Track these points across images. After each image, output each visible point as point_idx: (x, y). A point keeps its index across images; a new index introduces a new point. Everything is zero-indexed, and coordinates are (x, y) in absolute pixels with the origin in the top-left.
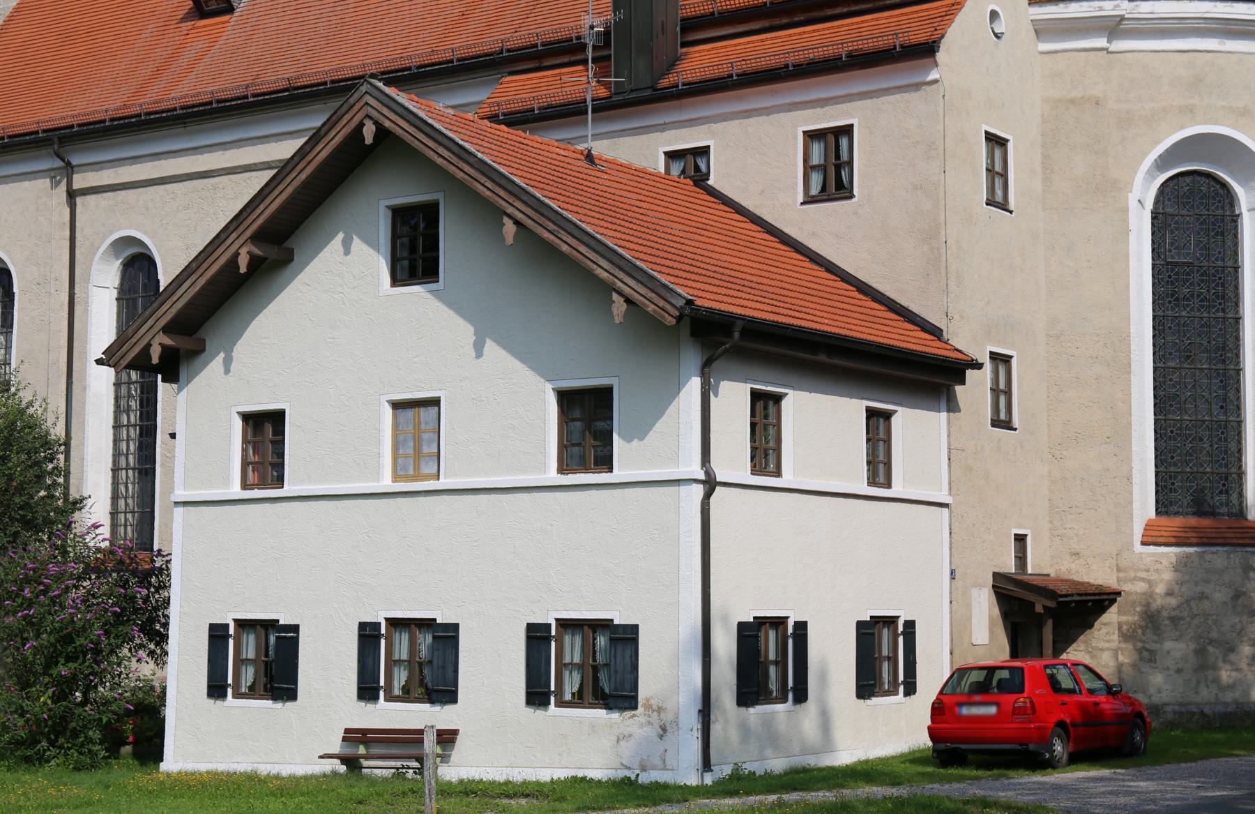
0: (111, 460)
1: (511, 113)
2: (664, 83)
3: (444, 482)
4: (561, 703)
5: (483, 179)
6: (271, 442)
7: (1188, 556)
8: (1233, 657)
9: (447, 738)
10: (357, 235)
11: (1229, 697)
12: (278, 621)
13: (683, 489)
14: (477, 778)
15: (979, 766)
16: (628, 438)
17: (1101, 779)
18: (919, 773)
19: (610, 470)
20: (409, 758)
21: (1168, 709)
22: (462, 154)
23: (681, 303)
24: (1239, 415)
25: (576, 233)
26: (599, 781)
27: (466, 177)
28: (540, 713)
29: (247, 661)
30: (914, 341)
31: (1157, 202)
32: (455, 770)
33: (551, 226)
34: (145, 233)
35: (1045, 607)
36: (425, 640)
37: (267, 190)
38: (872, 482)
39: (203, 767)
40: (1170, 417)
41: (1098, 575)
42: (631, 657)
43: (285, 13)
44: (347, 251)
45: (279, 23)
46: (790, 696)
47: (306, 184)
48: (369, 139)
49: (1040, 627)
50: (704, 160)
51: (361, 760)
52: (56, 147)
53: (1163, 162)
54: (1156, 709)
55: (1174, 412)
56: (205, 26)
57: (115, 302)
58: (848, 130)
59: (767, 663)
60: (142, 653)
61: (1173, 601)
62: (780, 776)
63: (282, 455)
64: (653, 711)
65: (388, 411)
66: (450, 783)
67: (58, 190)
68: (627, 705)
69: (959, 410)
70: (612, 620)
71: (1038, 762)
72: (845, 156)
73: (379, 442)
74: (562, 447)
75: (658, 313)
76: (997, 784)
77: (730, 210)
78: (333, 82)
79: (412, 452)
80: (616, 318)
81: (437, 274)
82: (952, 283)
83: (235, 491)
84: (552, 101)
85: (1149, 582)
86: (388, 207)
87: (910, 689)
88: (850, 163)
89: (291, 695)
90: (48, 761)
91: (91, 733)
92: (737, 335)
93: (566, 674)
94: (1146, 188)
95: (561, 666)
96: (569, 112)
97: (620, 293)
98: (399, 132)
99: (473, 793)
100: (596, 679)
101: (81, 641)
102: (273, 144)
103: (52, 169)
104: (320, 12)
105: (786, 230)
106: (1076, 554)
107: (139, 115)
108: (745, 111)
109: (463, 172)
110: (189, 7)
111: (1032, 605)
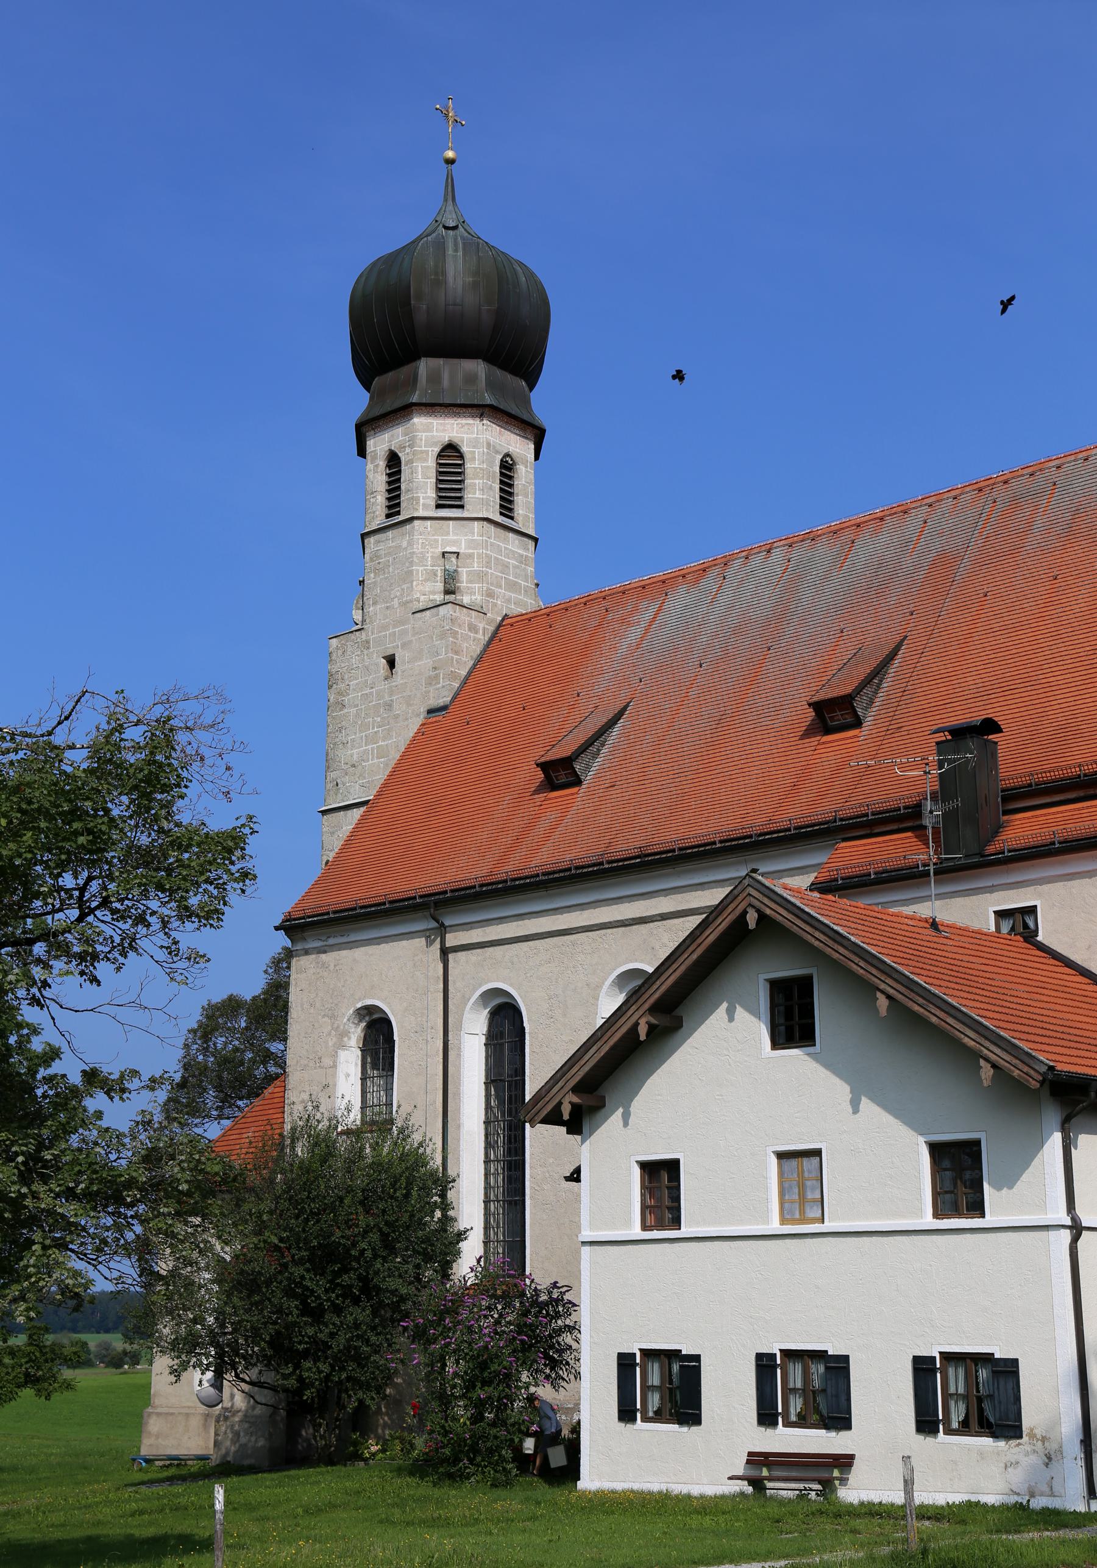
0: (482, 1192)
3: (829, 1226)
4: (949, 1431)
5: (857, 960)
9: (845, 1462)
10: (740, 1004)
12: (681, 1351)
13: (1052, 1234)
14: (876, 1500)
16: (998, 1188)
19: (983, 1215)
20: (813, 1480)
22: (837, 937)
23: (1044, 1069)
25: (945, 1007)
26: (993, 1506)
27: (841, 957)
28: (930, 1440)
29: (653, 1388)
33: (921, 1001)
34: (511, 985)
37: (663, 968)
39: (619, 1486)
42: (1013, 1389)
43: (629, 785)
44: (731, 1019)
45: (624, 794)
48: (752, 925)
50: (1032, 918)
51: (765, 1482)
52: (432, 910)
56: (556, 798)
57: (484, 1048)
60: (541, 1377)
63: (676, 1199)
64: (1038, 1440)
65: (774, 1160)
66: (851, 1504)
67: (432, 948)
68: (1012, 1434)
70: (993, 1354)
73: (767, 1189)
75: (1024, 1078)
77: (1060, 964)
78: (680, 849)
79: (797, 1197)
80: (984, 1081)
83: (636, 1231)
84: (888, 866)
86: (766, 980)
89: (694, 1419)
91: (504, 1452)
93: (952, 1404)
95: (946, 1396)
97: (987, 1060)
98: (779, 918)
99: (877, 1515)
100: (981, 1410)
101: (494, 1367)
102: (627, 904)
103: (428, 930)
104: (661, 783)
107: (505, 881)
108: (1068, 875)
109: (838, 953)
110: (540, 780)
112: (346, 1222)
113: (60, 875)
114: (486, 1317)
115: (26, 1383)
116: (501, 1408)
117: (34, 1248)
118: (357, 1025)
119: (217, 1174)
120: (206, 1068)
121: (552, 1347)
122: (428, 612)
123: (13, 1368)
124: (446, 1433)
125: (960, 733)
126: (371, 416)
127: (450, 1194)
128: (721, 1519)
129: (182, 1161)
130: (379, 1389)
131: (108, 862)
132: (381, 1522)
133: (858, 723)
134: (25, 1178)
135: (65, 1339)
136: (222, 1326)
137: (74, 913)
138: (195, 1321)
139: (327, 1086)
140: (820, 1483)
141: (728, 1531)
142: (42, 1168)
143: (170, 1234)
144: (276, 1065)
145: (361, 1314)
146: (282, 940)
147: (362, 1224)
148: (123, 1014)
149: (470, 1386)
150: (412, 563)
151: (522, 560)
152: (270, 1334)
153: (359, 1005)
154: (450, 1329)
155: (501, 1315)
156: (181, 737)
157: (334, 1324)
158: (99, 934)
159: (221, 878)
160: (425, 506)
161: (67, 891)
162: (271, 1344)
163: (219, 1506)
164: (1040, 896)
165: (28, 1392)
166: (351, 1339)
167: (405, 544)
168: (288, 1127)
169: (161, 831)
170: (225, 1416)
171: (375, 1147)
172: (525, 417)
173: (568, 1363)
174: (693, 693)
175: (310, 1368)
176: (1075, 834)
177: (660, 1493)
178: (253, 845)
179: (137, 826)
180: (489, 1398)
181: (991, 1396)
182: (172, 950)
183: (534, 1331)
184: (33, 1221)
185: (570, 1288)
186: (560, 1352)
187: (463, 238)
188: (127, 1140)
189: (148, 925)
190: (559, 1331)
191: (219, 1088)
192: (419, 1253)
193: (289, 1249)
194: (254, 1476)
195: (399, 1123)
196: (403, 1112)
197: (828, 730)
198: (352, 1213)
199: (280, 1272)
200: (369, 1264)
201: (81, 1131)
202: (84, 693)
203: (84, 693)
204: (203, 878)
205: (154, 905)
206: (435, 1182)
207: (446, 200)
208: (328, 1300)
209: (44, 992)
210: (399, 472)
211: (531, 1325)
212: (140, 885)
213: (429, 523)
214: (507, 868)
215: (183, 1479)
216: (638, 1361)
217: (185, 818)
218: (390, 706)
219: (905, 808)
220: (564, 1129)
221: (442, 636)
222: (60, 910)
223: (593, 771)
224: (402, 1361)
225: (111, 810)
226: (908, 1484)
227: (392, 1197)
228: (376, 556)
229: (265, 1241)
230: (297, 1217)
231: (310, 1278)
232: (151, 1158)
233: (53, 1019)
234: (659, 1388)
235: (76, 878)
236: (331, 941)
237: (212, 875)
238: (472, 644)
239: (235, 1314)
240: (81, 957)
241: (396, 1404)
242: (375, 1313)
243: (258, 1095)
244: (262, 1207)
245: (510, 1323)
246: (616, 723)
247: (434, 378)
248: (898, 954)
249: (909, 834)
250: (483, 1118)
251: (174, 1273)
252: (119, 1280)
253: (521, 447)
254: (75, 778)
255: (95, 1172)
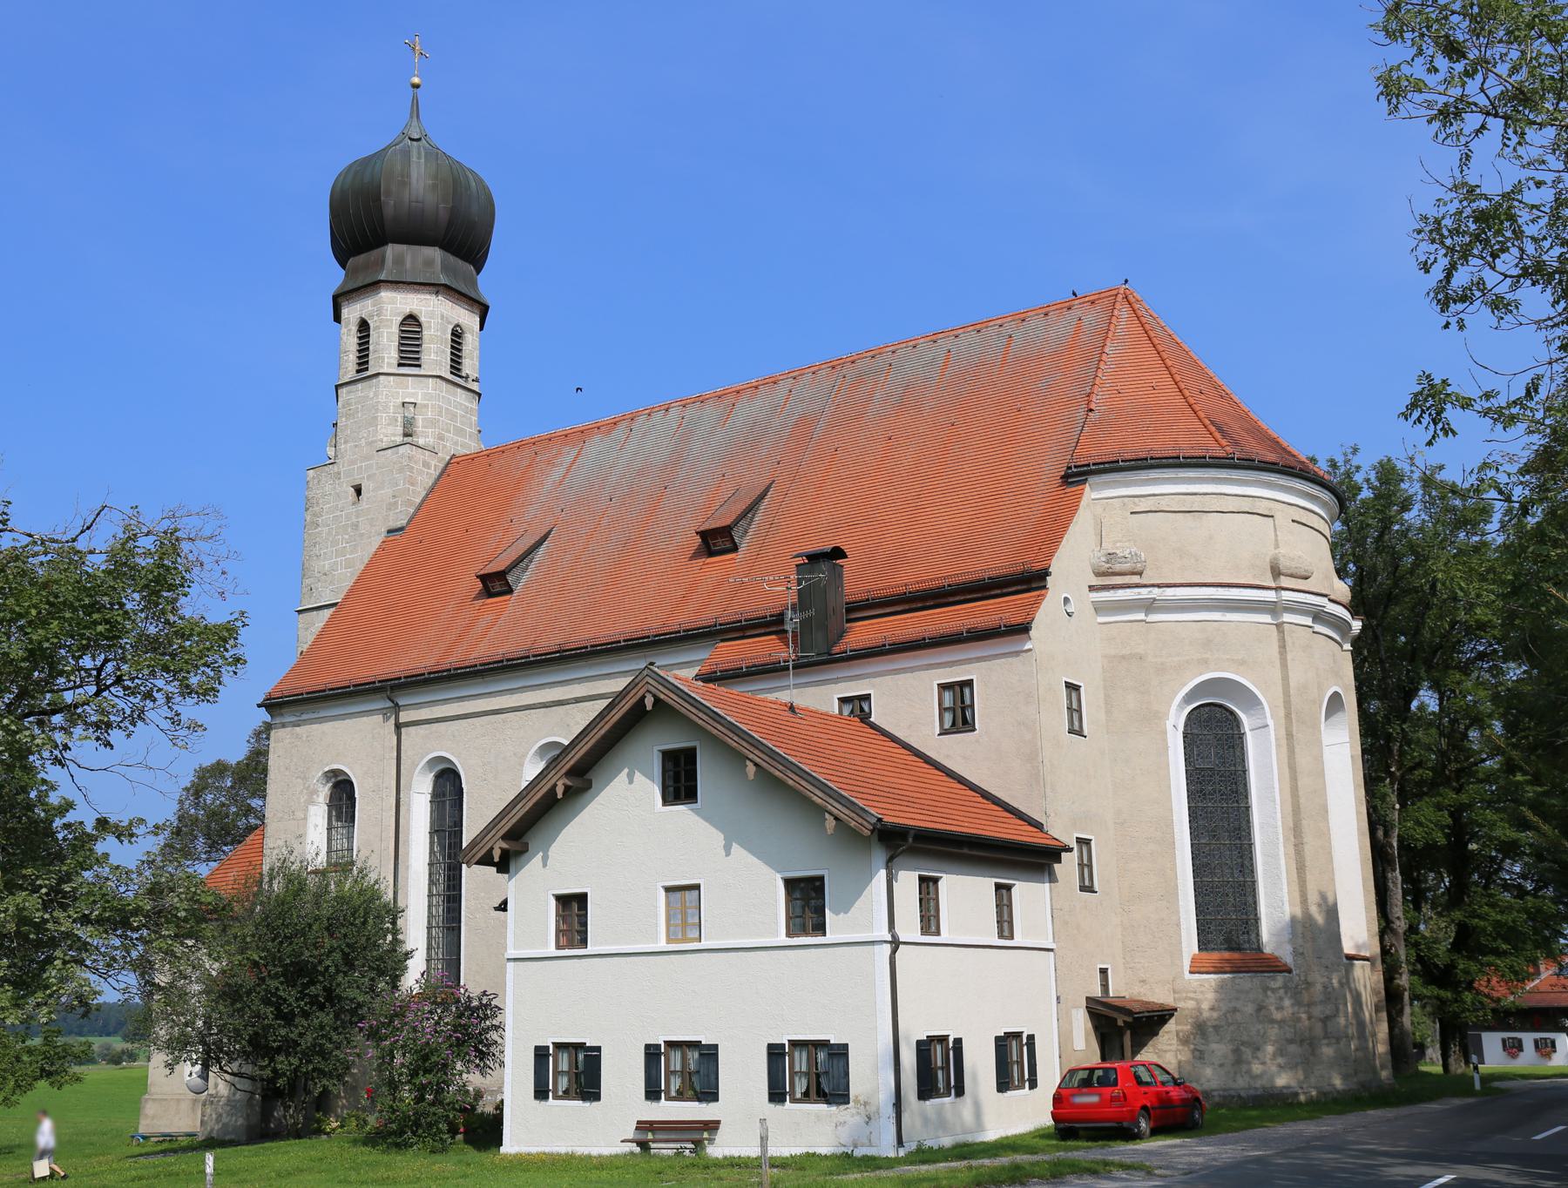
1: (726, 671)
2: (836, 649)
3: (704, 944)
4: (794, 1100)
5: (731, 735)
6: (578, 916)
7: (1223, 980)
8: (1259, 1054)
9: (712, 1126)
11: (1258, 1084)
13: (877, 947)
14: (736, 1155)
15: (1089, 1139)
16: (837, 913)
17: (1175, 1146)
18: (1048, 1145)
19: (824, 934)
20: (688, 1141)
21: (1215, 1093)
23: (874, 820)
24: (1253, 877)
28: (779, 1107)
30: (1024, 835)
31: (1186, 725)
32: (718, 1149)
33: (780, 767)
34: (453, 754)
35: (1124, 1022)
36: (693, 1056)
38: (1001, 936)
39: (534, 1150)
40: (1205, 879)
41: (1160, 996)
44: (631, 782)
46: (953, 1091)
47: (604, 737)
48: (649, 707)
49: (1121, 1035)
50: (867, 704)
53: (1188, 698)
54: (1207, 1094)
55: (1207, 876)
58: (969, 683)
59: (936, 1069)
60: (472, 1066)
61: (1215, 1015)
62: (948, 1150)
63: (585, 924)
65: (663, 893)
66: (717, 1159)
69: (1057, 881)
71: (1130, 1135)
72: (968, 702)
73: (656, 916)
74: (789, 918)
76: (1104, 1151)
78: (592, 646)
81: (697, 799)
82: (1048, 790)
83: (551, 950)
84: (756, 662)
85: (1196, 1000)
87: (1033, 1084)
88: (972, 706)
89: (596, 1097)
90: (411, 1147)
91: (441, 1126)
92: (910, 840)
93: (797, 1079)
94: (1178, 717)
96: (772, 670)
100: (818, 1084)
101: (434, 1059)
105: (928, 754)
106: (1143, 981)
107: (449, 670)
109: (716, 730)
111: (1116, 1019)
112: (314, 945)
113: (81, 657)
114: (428, 1019)
115: (42, 1076)
116: (439, 1091)
117: (55, 963)
118: (325, 785)
119: (210, 903)
120: (197, 819)
121: (481, 1042)
122: (390, 450)
123: (31, 1064)
124: (394, 1111)
125: (814, 558)
126: (346, 289)
127: (399, 922)
128: (615, 1173)
129: (181, 893)
130: (340, 1077)
131: (121, 647)
132: (340, 1182)
133: (735, 549)
134: (46, 906)
135: (75, 1041)
136: (210, 1028)
137: (92, 689)
138: (186, 1025)
139: (300, 836)
140: (693, 1142)
141: (620, 1181)
142: (62, 898)
143: (169, 952)
144: (257, 817)
145: (326, 1018)
146: (263, 715)
147: (327, 945)
148: (133, 773)
149: (414, 1074)
150: (377, 410)
151: (467, 410)
152: (249, 1034)
153: (326, 769)
154: (398, 1029)
155: (440, 1018)
156: (185, 547)
157: (302, 1026)
158: (113, 707)
159: (216, 662)
160: (389, 364)
161: (86, 670)
162: (250, 1042)
163: (209, 1169)
164: (873, 686)
165: (42, 1084)
166: (317, 1038)
167: (371, 395)
168: (266, 868)
169: (167, 622)
170: (212, 1101)
171: (339, 884)
172: (473, 295)
173: (494, 1055)
174: (605, 521)
175: (283, 1062)
176: (902, 638)
177: (567, 1154)
178: (244, 635)
179: (147, 618)
180: (430, 1083)
181: (826, 1073)
182: (175, 720)
183: (466, 1030)
184: (53, 943)
185: (496, 995)
186: (488, 1046)
187: (425, 148)
188: (134, 876)
189: (154, 700)
190: (487, 1030)
191: (208, 836)
192: (373, 969)
193: (265, 966)
194: (235, 1148)
195: (359, 864)
196: (362, 856)
197: (711, 554)
198: (319, 937)
199: (258, 985)
200: (333, 977)
201: (95, 867)
202: (104, 508)
203: (104, 508)
204: (203, 661)
205: (160, 683)
206: (387, 912)
207: (411, 117)
208: (298, 1006)
209: (64, 754)
210: (368, 336)
211: (465, 1025)
212: (148, 666)
213: (392, 378)
214: (450, 660)
215: (175, 1151)
216: (551, 1052)
217: (187, 612)
218: (357, 526)
219: (771, 616)
220: (494, 869)
221: (401, 470)
222: (81, 686)
223: (522, 582)
224: (358, 1055)
225: (124, 604)
226: (764, 1140)
227: (352, 924)
228: (348, 403)
229: (248, 959)
230: (273, 940)
231: (284, 990)
232: (155, 891)
233: (72, 776)
234: (567, 1073)
235: (94, 660)
236: (304, 717)
237: (210, 660)
238: (426, 478)
239: (221, 1019)
240: (97, 726)
241: (353, 1090)
242: (337, 1017)
243: (240, 842)
244: (246, 931)
245: (447, 1024)
246: (542, 544)
247: (399, 261)
248: (764, 731)
249: (774, 637)
250: (427, 861)
251: (172, 985)
252: (125, 991)
253: (469, 320)
254: (95, 577)
255: (108, 902)
